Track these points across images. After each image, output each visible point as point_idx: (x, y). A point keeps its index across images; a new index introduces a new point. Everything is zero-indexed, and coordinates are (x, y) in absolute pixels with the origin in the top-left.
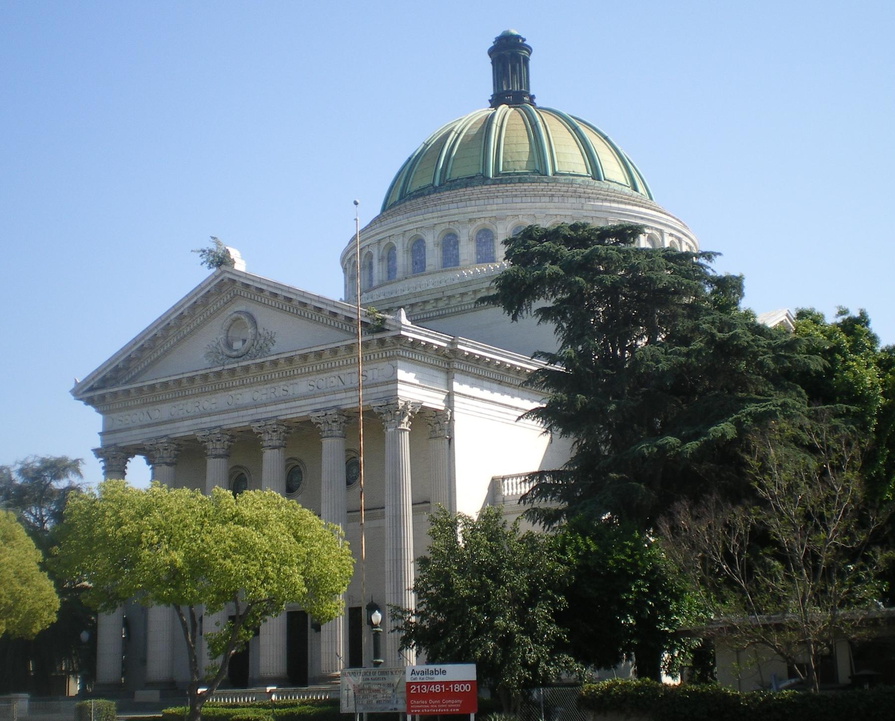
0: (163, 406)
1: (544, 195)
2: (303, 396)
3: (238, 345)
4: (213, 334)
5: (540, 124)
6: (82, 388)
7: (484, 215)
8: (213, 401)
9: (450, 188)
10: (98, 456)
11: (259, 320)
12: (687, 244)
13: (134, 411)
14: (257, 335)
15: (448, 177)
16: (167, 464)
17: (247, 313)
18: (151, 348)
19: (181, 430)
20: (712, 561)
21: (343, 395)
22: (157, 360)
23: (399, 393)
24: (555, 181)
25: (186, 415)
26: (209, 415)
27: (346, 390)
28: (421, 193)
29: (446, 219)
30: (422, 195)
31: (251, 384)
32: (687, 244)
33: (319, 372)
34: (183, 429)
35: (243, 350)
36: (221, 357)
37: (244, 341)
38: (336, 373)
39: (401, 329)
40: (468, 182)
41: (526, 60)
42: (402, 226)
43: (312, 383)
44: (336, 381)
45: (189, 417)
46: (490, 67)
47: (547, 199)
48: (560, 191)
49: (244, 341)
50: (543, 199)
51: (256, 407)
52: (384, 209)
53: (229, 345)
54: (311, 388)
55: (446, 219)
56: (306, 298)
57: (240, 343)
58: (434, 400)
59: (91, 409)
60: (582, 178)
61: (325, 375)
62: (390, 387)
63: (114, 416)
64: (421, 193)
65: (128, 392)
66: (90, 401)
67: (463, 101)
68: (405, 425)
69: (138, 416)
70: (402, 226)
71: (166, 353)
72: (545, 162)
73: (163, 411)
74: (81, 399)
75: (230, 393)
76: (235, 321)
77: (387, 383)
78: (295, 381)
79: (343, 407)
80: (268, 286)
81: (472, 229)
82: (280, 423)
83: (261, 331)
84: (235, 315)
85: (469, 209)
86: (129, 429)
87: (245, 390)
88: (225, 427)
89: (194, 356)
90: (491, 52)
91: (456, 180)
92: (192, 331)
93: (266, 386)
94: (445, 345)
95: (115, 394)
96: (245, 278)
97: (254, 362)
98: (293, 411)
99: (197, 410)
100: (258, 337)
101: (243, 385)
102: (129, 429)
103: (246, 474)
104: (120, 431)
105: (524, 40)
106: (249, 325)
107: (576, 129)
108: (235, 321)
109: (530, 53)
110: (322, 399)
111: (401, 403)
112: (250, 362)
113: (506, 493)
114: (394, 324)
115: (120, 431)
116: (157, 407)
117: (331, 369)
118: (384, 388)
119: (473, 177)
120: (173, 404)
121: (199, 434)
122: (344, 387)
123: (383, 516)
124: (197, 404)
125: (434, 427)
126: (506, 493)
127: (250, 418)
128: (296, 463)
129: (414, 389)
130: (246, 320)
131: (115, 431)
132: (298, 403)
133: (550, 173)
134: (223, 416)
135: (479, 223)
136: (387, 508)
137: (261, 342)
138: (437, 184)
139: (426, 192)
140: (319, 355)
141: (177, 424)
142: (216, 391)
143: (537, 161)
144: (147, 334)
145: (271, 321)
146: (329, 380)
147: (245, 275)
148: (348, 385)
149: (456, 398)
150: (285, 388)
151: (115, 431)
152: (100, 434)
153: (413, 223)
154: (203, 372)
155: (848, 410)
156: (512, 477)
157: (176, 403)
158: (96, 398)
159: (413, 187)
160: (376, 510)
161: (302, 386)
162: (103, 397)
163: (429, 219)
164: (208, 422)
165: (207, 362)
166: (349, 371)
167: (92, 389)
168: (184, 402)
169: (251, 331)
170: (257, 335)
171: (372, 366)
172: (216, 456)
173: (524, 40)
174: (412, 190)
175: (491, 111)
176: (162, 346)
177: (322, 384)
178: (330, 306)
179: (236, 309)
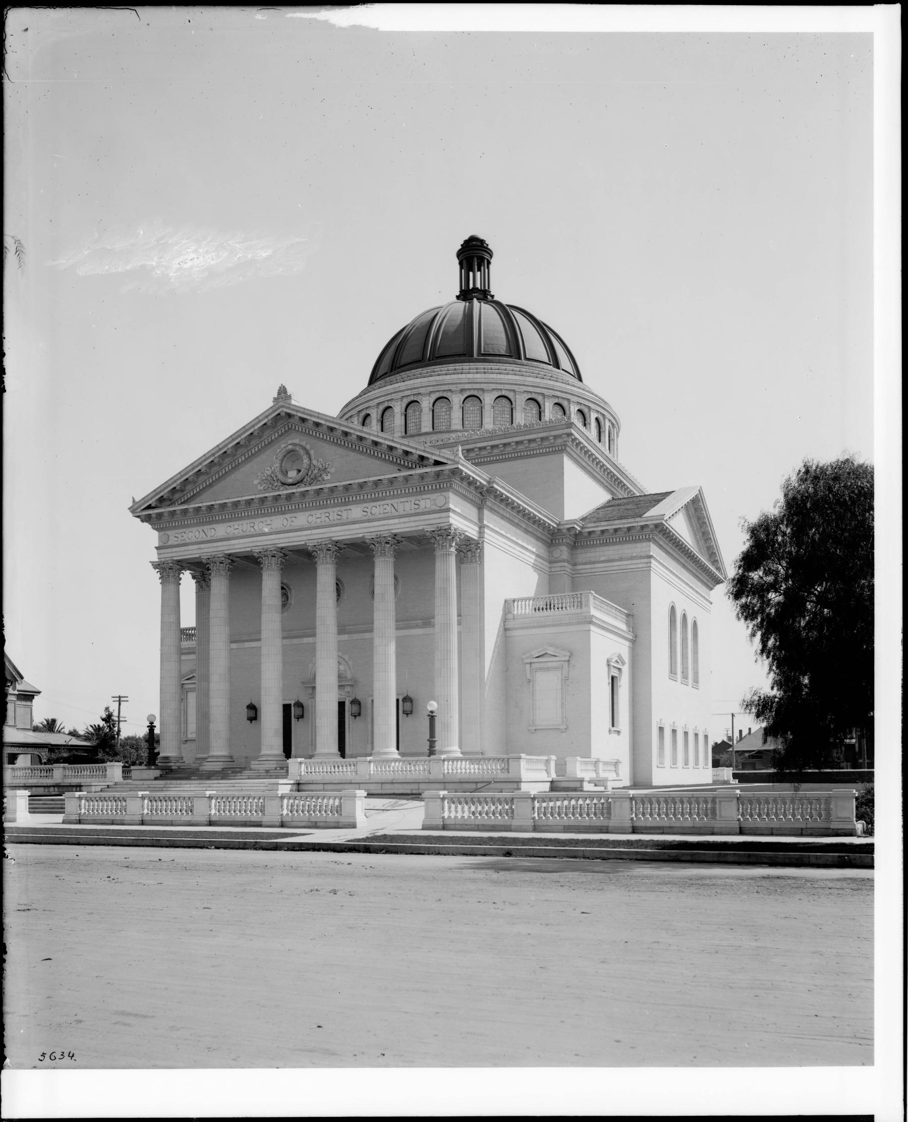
4: (269, 462)
6: (140, 507)
10: (155, 567)
12: (610, 420)
18: (207, 474)
19: (237, 547)
21: (396, 521)
32: (610, 420)
37: (299, 471)
39: (458, 463)
44: (389, 508)
49: (299, 471)
57: (295, 472)
58: (472, 532)
59: (147, 526)
65: (185, 511)
66: (147, 519)
67: (435, 290)
69: (174, 536)
73: (221, 530)
74: (138, 517)
78: (348, 507)
80: (326, 420)
90: (459, 254)
93: (321, 511)
94: (485, 483)
95: (173, 513)
99: (252, 529)
100: (312, 468)
108: (292, 451)
109: (491, 257)
112: (308, 488)
113: (515, 612)
125: (470, 551)
126: (515, 612)
129: (461, 518)
130: (302, 452)
144: (205, 460)
148: (401, 512)
149: (486, 530)
150: (417, 502)
152: (157, 548)
156: (522, 600)
160: (427, 621)
161: (356, 512)
162: (160, 515)
166: (402, 500)
167: (149, 507)
169: (306, 461)
171: (424, 497)
177: (374, 510)
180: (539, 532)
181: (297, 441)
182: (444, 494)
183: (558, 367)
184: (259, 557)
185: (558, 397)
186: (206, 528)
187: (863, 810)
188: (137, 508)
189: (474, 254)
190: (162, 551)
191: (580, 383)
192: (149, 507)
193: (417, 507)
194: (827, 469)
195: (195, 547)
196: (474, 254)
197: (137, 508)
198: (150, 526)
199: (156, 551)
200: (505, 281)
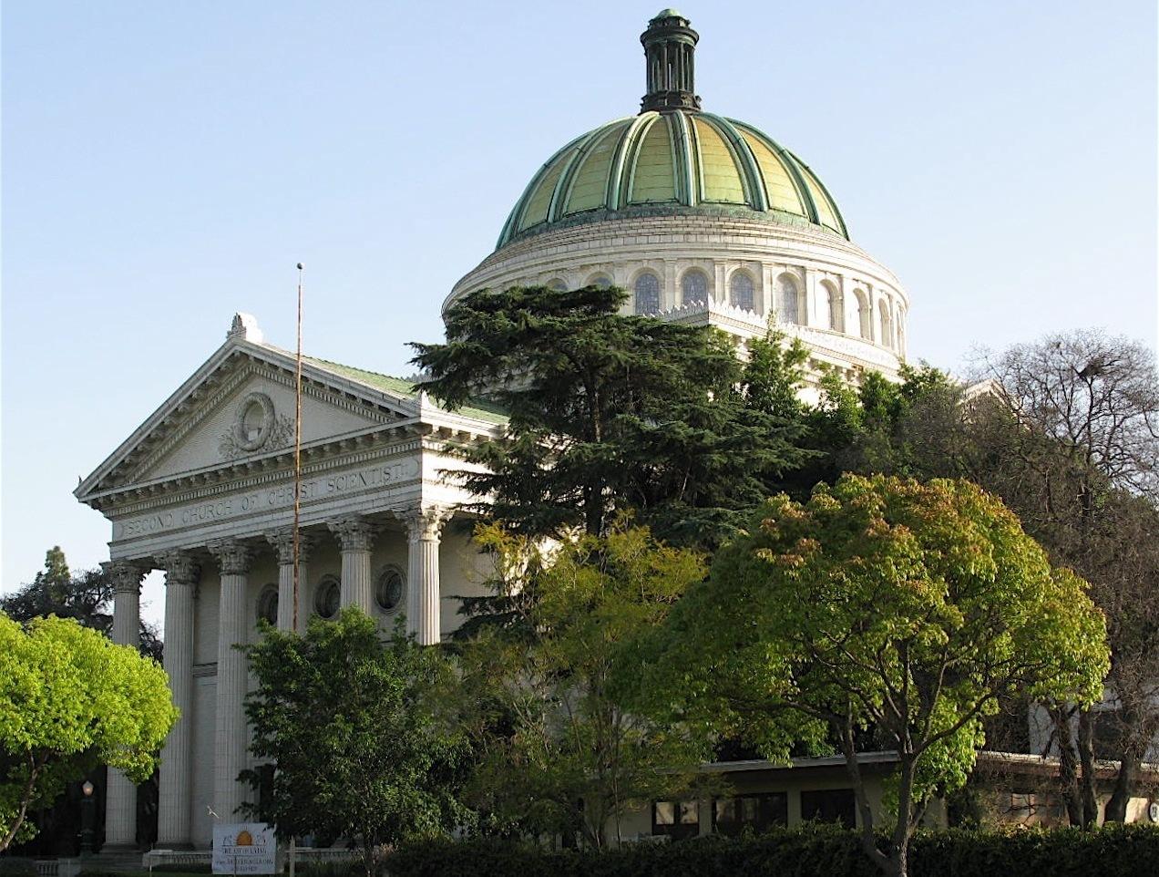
1: (677, 233)
3: (253, 435)
4: (227, 421)
5: (687, 137)
8: (228, 504)
11: (276, 404)
13: (143, 517)
14: (274, 422)
15: (564, 211)
16: (180, 582)
17: (264, 395)
19: (194, 540)
20: (810, 720)
21: (364, 498)
22: (168, 454)
23: (424, 494)
24: (699, 213)
27: (367, 492)
28: (531, 232)
29: (551, 267)
30: (533, 234)
31: (267, 484)
33: (337, 469)
34: (195, 539)
35: (258, 442)
36: (235, 450)
37: (260, 429)
38: (357, 471)
40: (653, 209)
41: (689, 49)
42: (500, 275)
43: (332, 483)
45: (204, 523)
46: (644, 60)
47: (681, 238)
48: (700, 226)
49: (260, 429)
50: (676, 238)
51: (272, 511)
52: (499, 247)
53: (244, 436)
54: (331, 489)
55: (551, 267)
56: (321, 377)
60: (737, 208)
61: (345, 473)
62: (415, 488)
63: (125, 522)
64: (531, 232)
66: (95, 505)
68: (433, 537)
69: (147, 524)
70: (500, 275)
71: (178, 445)
72: (687, 186)
73: (175, 517)
74: (85, 502)
75: (246, 495)
77: (411, 483)
81: (679, 272)
83: (278, 418)
85: (580, 254)
86: (140, 538)
87: (260, 491)
88: (238, 537)
89: (205, 451)
90: (644, 39)
91: (574, 214)
97: (266, 456)
98: (311, 517)
102: (140, 538)
104: (131, 540)
105: (687, 23)
107: (736, 143)
110: (342, 503)
111: (424, 506)
114: (412, 408)
115: (131, 540)
116: (169, 511)
117: (351, 466)
119: (595, 210)
120: (183, 508)
121: (211, 546)
122: (366, 488)
124: (210, 508)
133: (693, 202)
135: (593, 270)
137: (278, 431)
138: (550, 220)
139: (537, 230)
140: (336, 447)
141: (190, 533)
142: (229, 493)
143: (677, 188)
145: (285, 402)
146: (349, 481)
147: (258, 349)
151: (125, 541)
155: (469, 509)
157: (188, 507)
158: (101, 501)
163: (682, 250)
164: (223, 531)
165: (221, 456)
167: (96, 489)
170: (274, 422)
172: (230, 573)
173: (687, 23)
176: (173, 437)
178: (346, 386)
179: (253, 390)
180: (206, 595)
181: (260, 389)
183: (816, 222)
185: (785, 265)
186: (162, 514)
187: (718, 865)
188: (83, 492)
189: (667, 44)
192: (96, 489)
193: (387, 477)
194: (443, 526)
196: (667, 44)
197: (83, 492)
198: (101, 514)
199: (108, 547)
200: (716, 83)
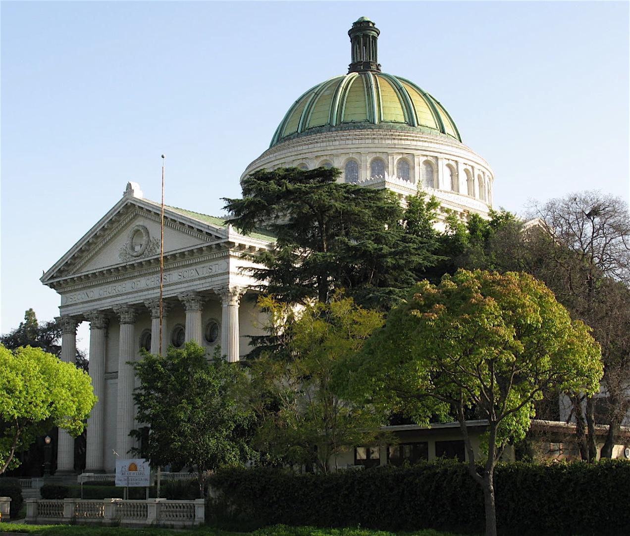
0: (95, 289)
1: (368, 138)
2: (181, 282)
3: (137, 248)
4: (123, 240)
7: (326, 153)
8: (124, 286)
9: (307, 134)
11: (150, 231)
14: (149, 241)
15: (307, 126)
16: (98, 328)
19: (106, 305)
21: (198, 282)
22: (92, 258)
23: (231, 280)
24: (380, 127)
25: (109, 295)
26: (121, 295)
27: (199, 279)
28: (289, 138)
31: (145, 275)
33: (183, 266)
34: (106, 305)
35: (140, 252)
36: (128, 256)
37: (141, 245)
38: (194, 267)
40: (355, 125)
42: (272, 161)
43: (180, 274)
44: (194, 272)
45: (111, 296)
46: (350, 44)
47: (370, 141)
48: (380, 135)
49: (141, 245)
50: (367, 141)
51: (148, 290)
52: (271, 146)
53: (133, 249)
54: (180, 277)
56: (175, 216)
60: (401, 125)
61: (188, 268)
62: (225, 277)
63: (68, 295)
64: (289, 138)
66: (52, 286)
69: (79, 296)
70: (272, 161)
71: (96, 254)
72: (374, 113)
73: (95, 293)
74: (46, 285)
75: (134, 280)
76: (137, 232)
77: (223, 274)
79: (198, 290)
82: (199, 293)
83: (151, 239)
84: (136, 228)
86: (76, 304)
89: (111, 257)
90: (350, 33)
92: (111, 238)
96: (140, 203)
97: (144, 260)
98: (169, 293)
101: (140, 275)
102: (76, 304)
103: (218, 324)
105: (374, 24)
106: (144, 234)
107: (400, 89)
110: (186, 285)
111: (231, 287)
115: (71, 305)
117: (191, 265)
118: (222, 277)
119: (323, 126)
120: (99, 288)
122: (199, 277)
123: (117, 377)
124: (114, 288)
127: (144, 297)
128: (215, 322)
131: (68, 306)
132: (172, 288)
133: (377, 121)
134: (129, 296)
135: (322, 159)
136: (119, 373)
137: (151, 246)
138: (299, 131)
139: (292, 137)
140: (182, 254)
141: (103, 301)
142: (125, 279)
143: (368, 114)
146: (190, 273)
147: (140, 201)
151: (68, 306)
153: (279, 159)
154: (116, 267)
158: (55, 284)
159: (286, 133)
161: (174, 276)
167: (52, 277)
168: (107, 286)
170: (149, 241)
173: (374, 24)
174: (286, 135)
175: (345, 75)
176: (94, 249)
179: (138, 224)
181: (141, 223)
182: (226, 260)
183: (443, 132)
184: (149, 307)
185: (427, 156)
186: (88, 291)
188: (45, 279)
189: (363, 36)
190: (62, 310)
191: (460, 144)
192: (52, 277)
193: (210, 271)
195: (81, 306)
196: (363, 36)
197: (45, 279)
199: (59, 309)
200: (389, 57)
